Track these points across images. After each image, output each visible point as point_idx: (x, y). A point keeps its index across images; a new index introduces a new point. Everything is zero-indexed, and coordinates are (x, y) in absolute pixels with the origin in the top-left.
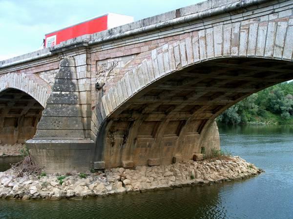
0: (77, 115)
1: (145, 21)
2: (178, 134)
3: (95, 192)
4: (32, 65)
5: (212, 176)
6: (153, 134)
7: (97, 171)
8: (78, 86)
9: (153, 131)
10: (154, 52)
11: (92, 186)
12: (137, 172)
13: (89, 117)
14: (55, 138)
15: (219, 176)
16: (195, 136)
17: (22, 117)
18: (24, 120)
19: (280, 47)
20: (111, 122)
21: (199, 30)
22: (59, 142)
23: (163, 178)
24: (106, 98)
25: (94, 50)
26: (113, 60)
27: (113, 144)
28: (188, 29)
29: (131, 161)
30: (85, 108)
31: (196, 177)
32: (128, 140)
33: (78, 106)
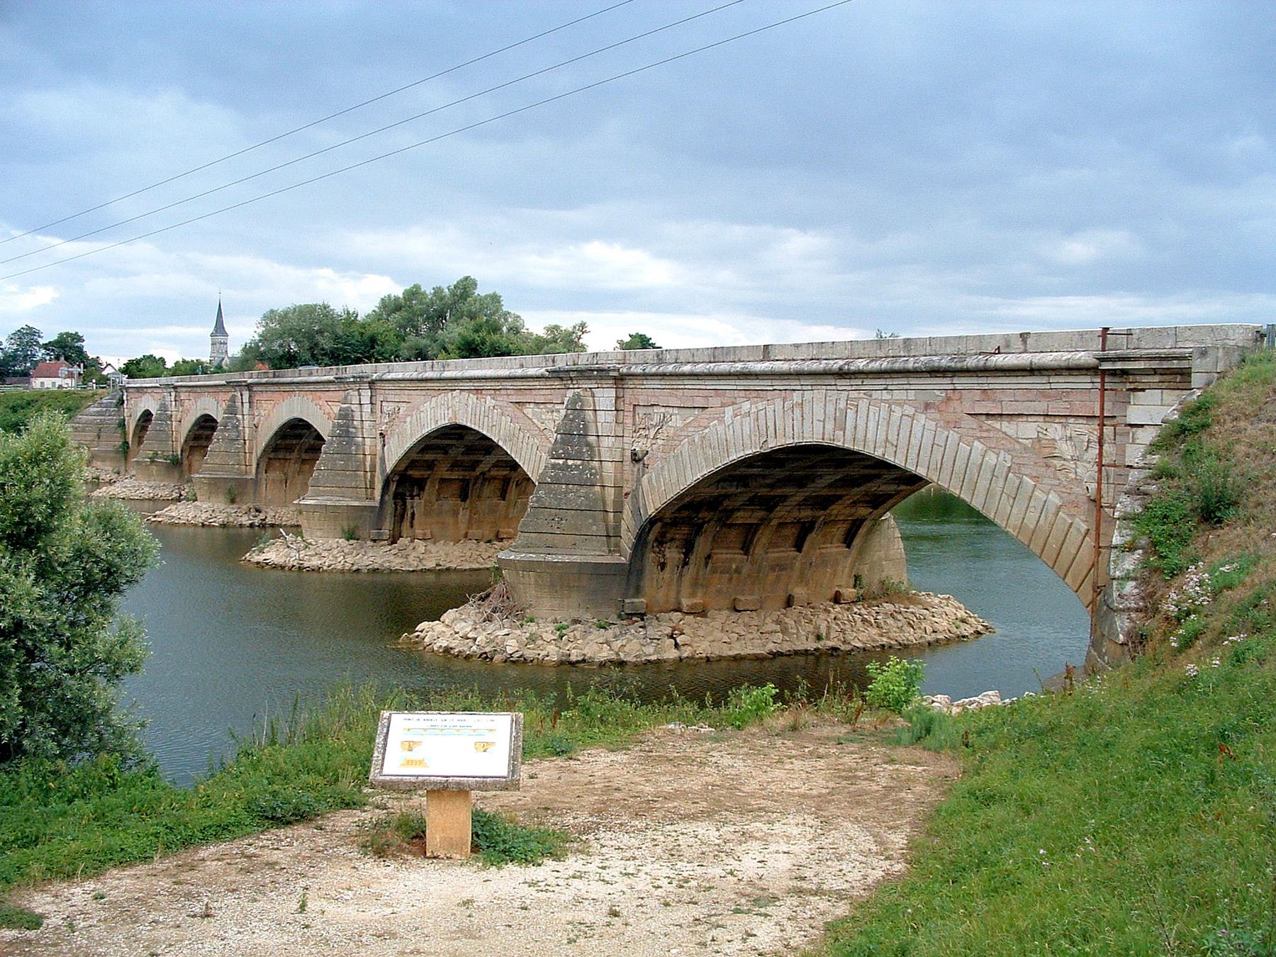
0: (595, 508)
1: (717, 352)
2: (799, 546)
3: (622, 655)
4: (508, 384)
5: (862, 637)
6: (746, 548)
7: (630, 616)
9: (745, 542)
10: (729, 411)
11: (617, 644)
12: (707, 624)
13: (618, 512)
14: (552, 551)
15: (877, 638)
16: (838, 553)
17: (477, 478)
18: (482, 484)
20: (659, 525)
22: (560, 558)
23: (757, 635)
24: (650, 481)
25: (630, 383)
26: (663, 410)
27: (663, 566)
29: (698, 600)
30: (610, 494)
31: (828, 638)
32: (693, 558)
33: (597, 489)
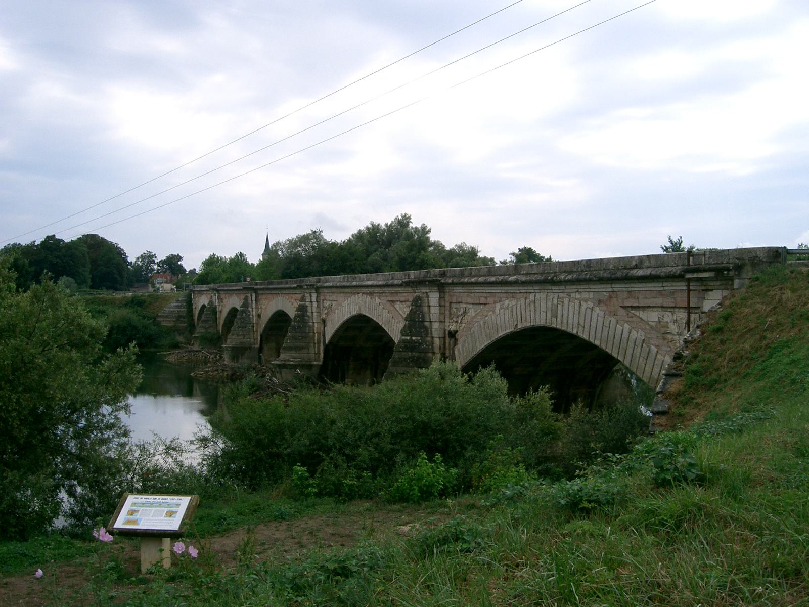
8: (431, 331)
10: (498, 306)
19: (535, 295)
21: (531, 293)
28: (523, 289)
